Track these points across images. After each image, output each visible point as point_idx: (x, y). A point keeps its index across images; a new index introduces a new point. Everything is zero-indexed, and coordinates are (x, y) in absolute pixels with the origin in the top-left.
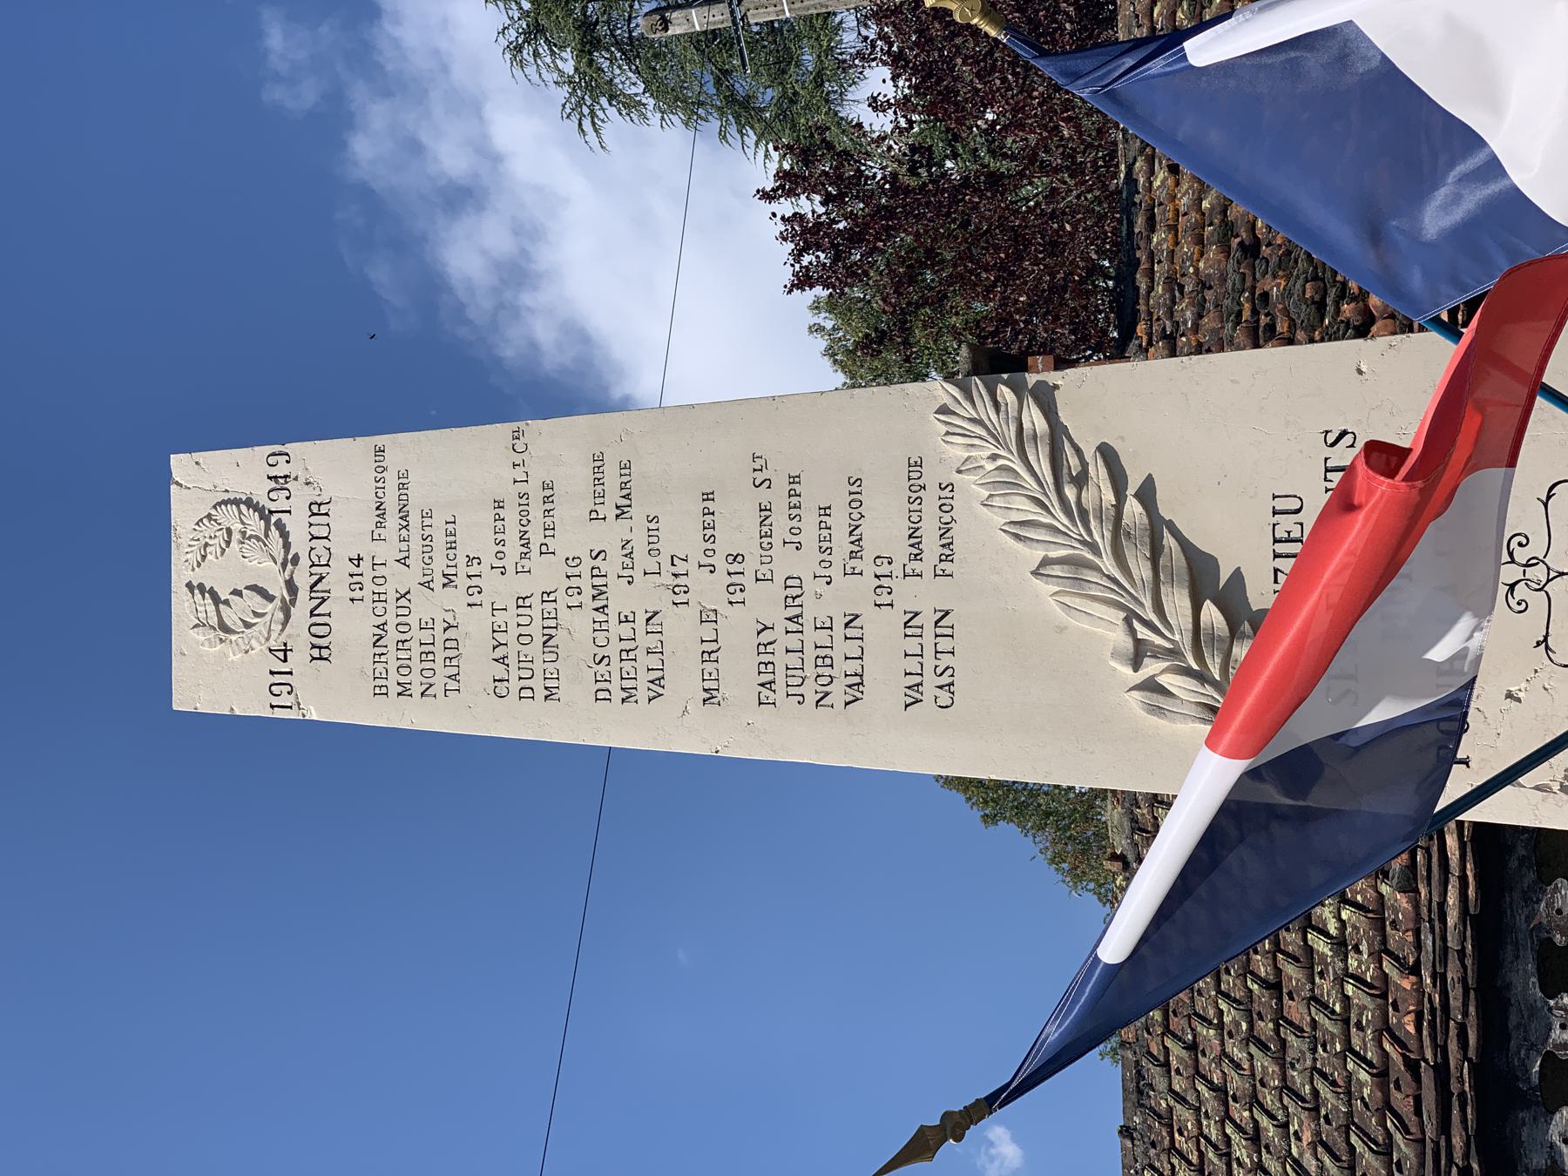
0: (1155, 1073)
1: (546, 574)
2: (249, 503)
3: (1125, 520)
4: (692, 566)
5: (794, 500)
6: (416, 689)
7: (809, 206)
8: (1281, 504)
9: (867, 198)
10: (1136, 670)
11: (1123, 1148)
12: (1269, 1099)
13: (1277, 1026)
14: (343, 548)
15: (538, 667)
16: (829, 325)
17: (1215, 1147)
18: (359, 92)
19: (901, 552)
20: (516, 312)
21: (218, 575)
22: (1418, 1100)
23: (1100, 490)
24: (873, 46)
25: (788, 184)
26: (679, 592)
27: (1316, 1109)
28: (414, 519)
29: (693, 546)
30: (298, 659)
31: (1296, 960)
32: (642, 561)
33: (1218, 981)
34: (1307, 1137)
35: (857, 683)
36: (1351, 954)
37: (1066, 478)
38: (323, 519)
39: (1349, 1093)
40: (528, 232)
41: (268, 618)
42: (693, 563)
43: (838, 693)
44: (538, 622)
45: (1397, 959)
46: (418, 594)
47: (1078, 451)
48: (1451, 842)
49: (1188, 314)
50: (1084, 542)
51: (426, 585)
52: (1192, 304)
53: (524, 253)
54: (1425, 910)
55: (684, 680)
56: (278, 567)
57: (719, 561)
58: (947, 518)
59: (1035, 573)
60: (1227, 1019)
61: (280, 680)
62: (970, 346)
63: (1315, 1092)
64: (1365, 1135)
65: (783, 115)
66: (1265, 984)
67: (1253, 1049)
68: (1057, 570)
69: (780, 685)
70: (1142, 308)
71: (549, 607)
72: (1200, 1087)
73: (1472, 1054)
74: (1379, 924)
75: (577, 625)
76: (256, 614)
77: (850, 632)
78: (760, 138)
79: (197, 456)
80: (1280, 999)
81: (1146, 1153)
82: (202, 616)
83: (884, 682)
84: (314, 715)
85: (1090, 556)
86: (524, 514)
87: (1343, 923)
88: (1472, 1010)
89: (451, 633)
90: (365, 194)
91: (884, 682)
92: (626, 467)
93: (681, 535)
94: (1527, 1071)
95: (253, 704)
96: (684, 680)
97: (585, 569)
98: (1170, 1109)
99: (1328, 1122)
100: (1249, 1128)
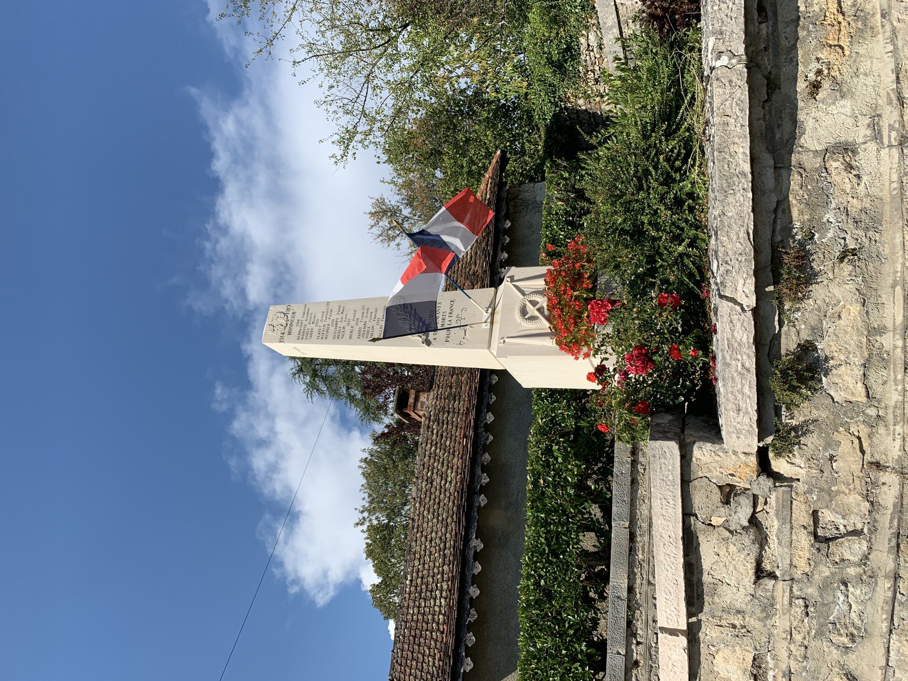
1: (329, 322)
16: (364, 466)
18: (239, 409)
20: (270, 479)
32: (344, 319)
40: (280, 456)
53: (277, 462)
75: (332, 329)
90: (234, 438)
93: (350, 316)
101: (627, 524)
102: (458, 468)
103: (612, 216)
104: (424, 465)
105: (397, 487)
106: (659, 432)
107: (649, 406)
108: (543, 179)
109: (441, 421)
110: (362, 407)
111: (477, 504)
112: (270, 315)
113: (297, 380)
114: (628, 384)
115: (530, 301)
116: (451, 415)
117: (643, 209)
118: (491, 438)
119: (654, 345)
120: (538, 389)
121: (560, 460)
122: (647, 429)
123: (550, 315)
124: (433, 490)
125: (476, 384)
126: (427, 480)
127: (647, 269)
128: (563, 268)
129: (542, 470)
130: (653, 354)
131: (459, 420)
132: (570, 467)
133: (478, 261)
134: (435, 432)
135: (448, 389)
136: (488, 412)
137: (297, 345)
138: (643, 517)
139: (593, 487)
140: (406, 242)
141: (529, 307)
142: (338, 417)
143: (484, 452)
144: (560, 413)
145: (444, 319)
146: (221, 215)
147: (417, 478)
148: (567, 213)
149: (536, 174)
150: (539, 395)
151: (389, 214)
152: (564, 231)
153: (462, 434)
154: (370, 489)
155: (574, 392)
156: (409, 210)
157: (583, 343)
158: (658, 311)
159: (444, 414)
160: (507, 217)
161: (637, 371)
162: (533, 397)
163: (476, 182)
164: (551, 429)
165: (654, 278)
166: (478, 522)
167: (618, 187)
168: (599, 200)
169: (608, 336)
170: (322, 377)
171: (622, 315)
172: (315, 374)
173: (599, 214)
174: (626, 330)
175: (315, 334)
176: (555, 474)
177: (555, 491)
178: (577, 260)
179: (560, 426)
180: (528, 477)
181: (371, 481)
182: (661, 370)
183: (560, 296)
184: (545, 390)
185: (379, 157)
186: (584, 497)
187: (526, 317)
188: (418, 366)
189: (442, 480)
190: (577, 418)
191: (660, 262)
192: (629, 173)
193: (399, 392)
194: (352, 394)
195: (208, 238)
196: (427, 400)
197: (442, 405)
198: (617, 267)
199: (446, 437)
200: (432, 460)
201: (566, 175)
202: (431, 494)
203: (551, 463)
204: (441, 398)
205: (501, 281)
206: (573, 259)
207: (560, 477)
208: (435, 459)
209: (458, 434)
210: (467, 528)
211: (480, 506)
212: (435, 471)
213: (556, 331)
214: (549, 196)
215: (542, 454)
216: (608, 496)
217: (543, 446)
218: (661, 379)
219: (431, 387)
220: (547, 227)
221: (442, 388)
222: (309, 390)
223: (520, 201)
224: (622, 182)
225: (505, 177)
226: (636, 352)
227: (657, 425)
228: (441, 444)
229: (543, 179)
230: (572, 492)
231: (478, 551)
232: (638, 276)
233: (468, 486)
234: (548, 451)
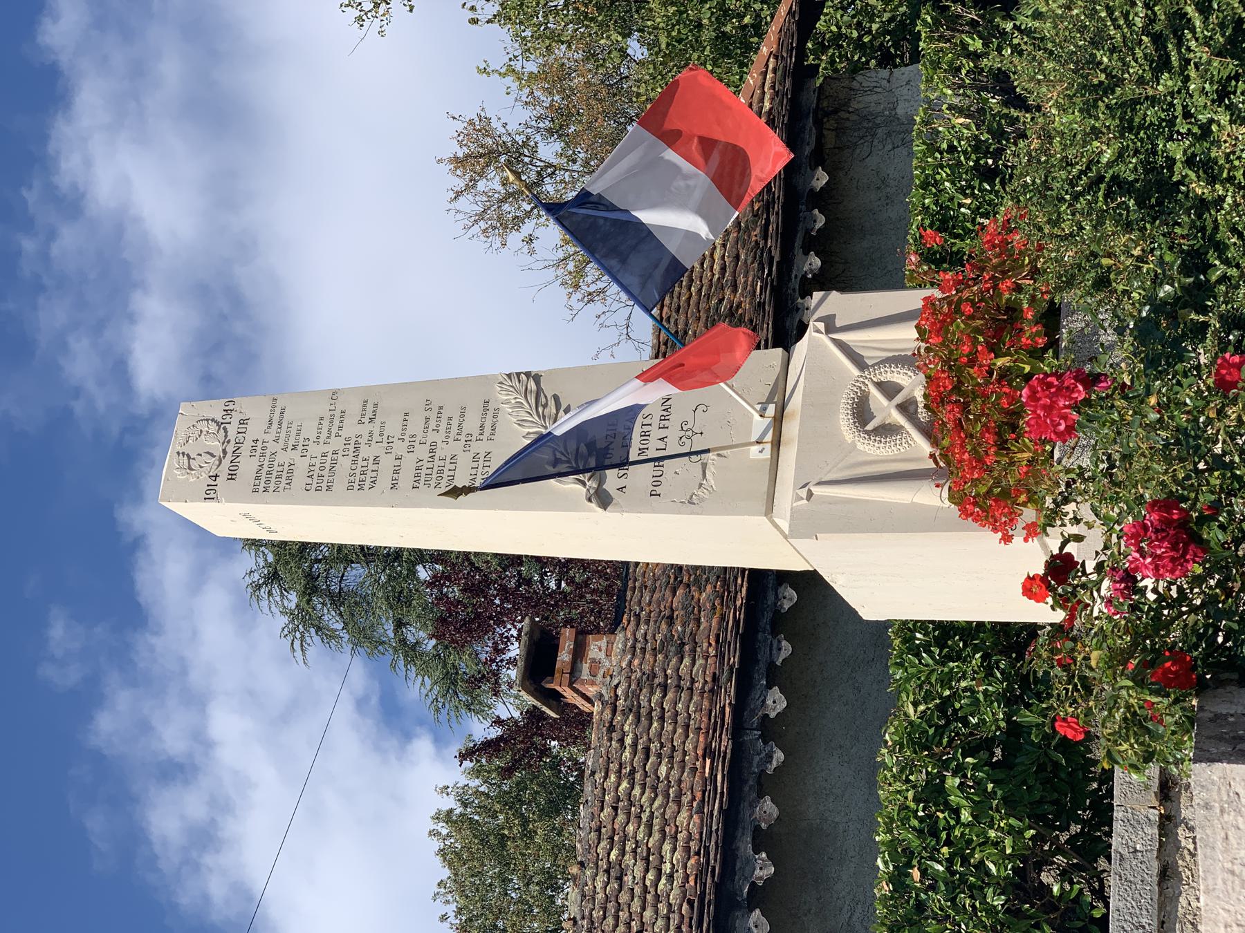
1: (337, 443)
14: (250, 437)
16: (444, 832)
19: (476, 433)
20: (197, 867)
28: (284, 425)
32: (376, 438)
40: (221, 805)
42: (396, 438)
53: (213, 822)
57: (407, 438)
75: (345, 463)
86: (331, 422)
89: (291, 467)
92: (376, 405)
93: (393, 428)
97: (352, 442)
102: (690, 837)
103: (1085, 143)
104: (599, 830)
105: (534, 888)
106: (1220, 738)
107: (1195, 667)
108: (916, 57)
109: (643, 712)
110: (438, 674)
112: (181, 426)
113: (264, 603)
114: (1134, 608)
115: (880, 385)
116: (670, 695)
117: (1171, 123)
118: (779, 756)
119: (1206, 498)
120: (905, 622)
121: (965, 816)
122: (1188, 731)
123: (932, 423)
124: (624, 898)
125: (737, 610)
126: (607, 871)
127: (1183, 288)
128: (966, 294)
129: (916, 843)
130: (1202, 520)
131: (692, 708)
132: (992, 834)
133: (741, 279)
134: (628, 741)
135: (664, 626)
136: (769, 686)
137: (256, 509)
139: (1056, 889)
140: (550, 234)
141: (877, 399)
142: (374, 700)
143: (761, 796)
144: (965, 690)
145: (645, 435)
146: (64, 166)
147: (582, 864)
148: (978, 146)
149: (896, 45)
150: (909, 640)
151: (503, 159)
152: (973, 195)
153: (701, 745)
154: (462, 893)
155: (1003, 629)
156: (558, 146)
157: (1023, 498)
158: (1217, 402)
159: (652, 693)
160: (819, 158)
161: (1157, 568)
162: (890, 646)
163: (735, 68)
164: (940, 731)
165: (1204, 310)
167: (1100, 63)
168: (1050, 97)
169: (1081, 475)
170: (331, 595)
171: (1115, 416)
172: (311, 588)
173: (1050, 138)
174: (1127, 458)
175: (300, 478)
176: (952, 855)
177: (953, 900)
178: (1004, 273)
179: (966, 723)
180: (879, 862)
181: (463, 870)
182: (1227, 567)
183: (960, 370)
184: (922, 625)
185: (473, 8)
186: (1031, 917)
187: (870, 427)
188: (584, 564)
189: (647, 871)
190: (1011, 701)
191: (1220, 269)
192: (1130, 25)
193: (531, 634)
194: (411, 639)
195: (27, 225)
196: (608, 655)
197: (647, 668)
198: (1102, 282)
199: (659, 756)
200: (621, 818)
201: (976, 45)
202: (619, 907)
203: (942, 824)
204: (644, 650)
205: (802, 329)
206: (995, 268)
207: (965, 861)
208: (629, 814)
209: (689, 746)
212: (630, 846)
213: (948, 464)
214: (929, 101)
215: (917, 800)
216: (1097, 914)
217: (919, 778)
218: (1228, 592)
220: (925, 185)
221: (647, 622)
222: (296, 628)
223: (854, 117)
224: (1113, 50)
225: (813, 52)
226: (1154, 517)
227: (1217, 718)
228: (646, 774)
229: (916, 57)
230: (998, 902)
232: (1159, 307)
233: (718, 887)
234: (933, 793)
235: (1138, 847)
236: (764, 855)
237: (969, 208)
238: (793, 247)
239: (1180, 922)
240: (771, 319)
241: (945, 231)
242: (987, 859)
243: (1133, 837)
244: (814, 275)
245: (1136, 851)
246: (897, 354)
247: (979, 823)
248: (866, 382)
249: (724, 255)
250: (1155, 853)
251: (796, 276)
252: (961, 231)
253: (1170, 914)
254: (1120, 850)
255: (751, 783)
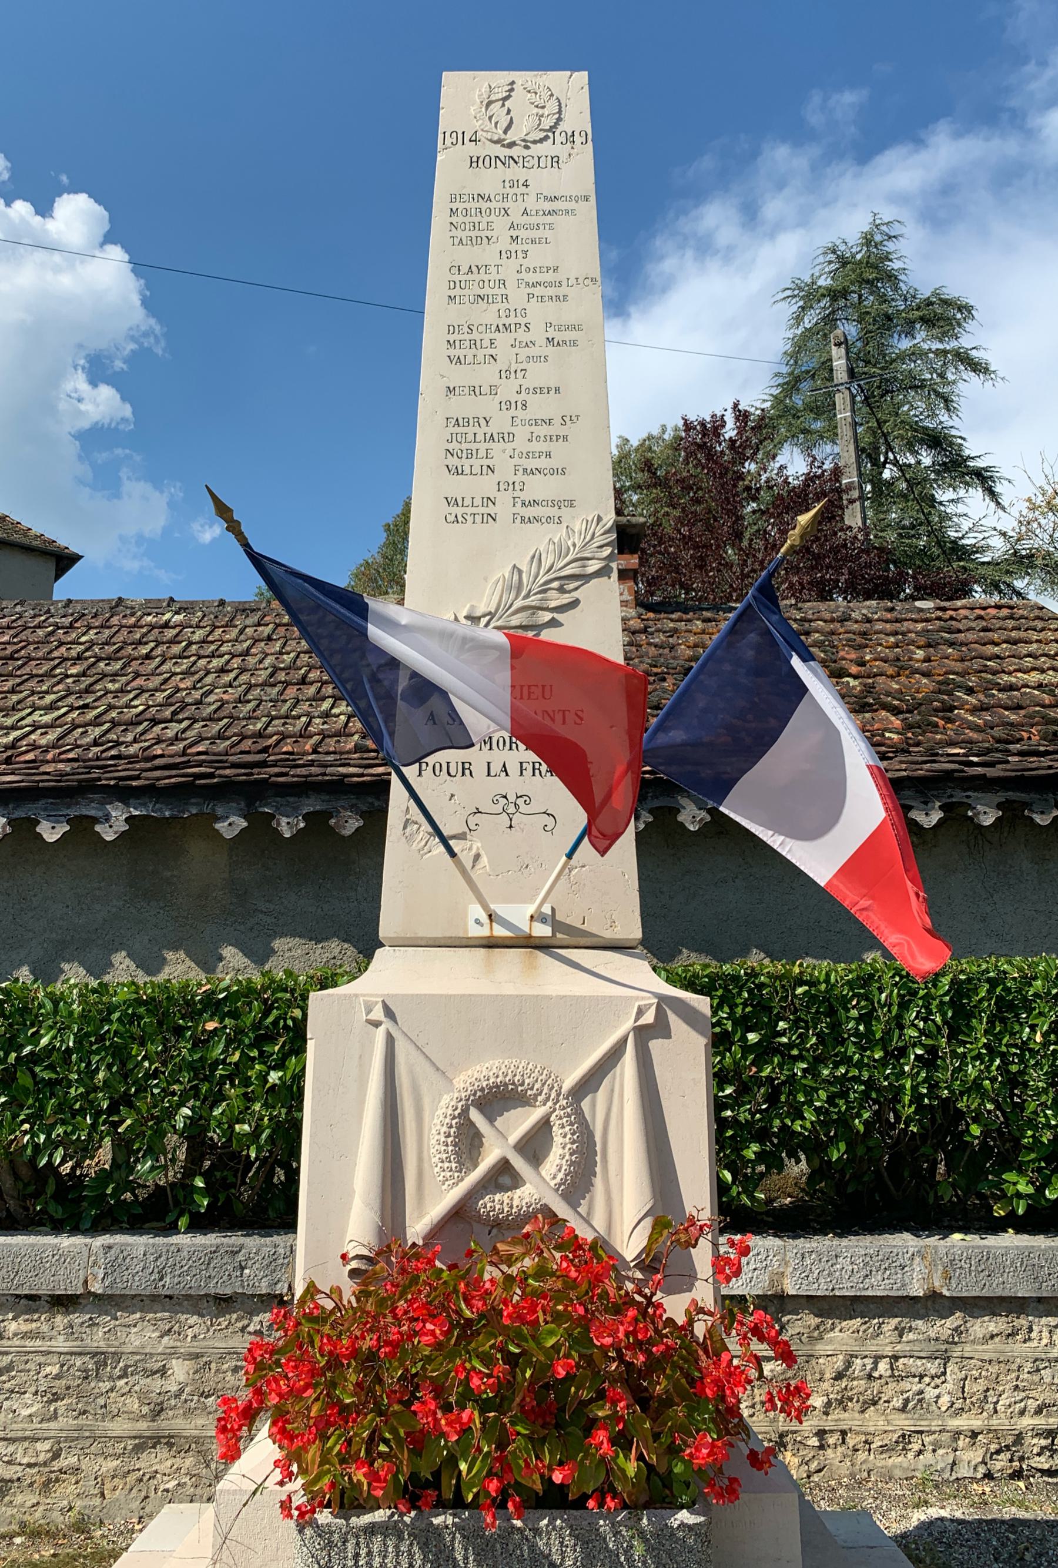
0: (254, 618)
1: (517, 296)
2: (559, 119)
3: (540, 612)
4: (521, 381)
5: (554, 438)
6: (454, 220)
7: (730, 431)
8: (547, 689)
9: (733, 462)
10: (465, 617)
11: (213, 601)
12: (244, 677)
13: (283, 683)
15: (466, 292)
16: (666, 437)
17: (217, 650)
18: (815, 151)
19: (526, 496)
20: (682, 247)
21: (519, 101)
22: (248, 752)
23: (556, 600)
24: (819, 467)
25: (742, 416)
26: (507, 373)
27: (240, 702)
28: (549, 219)
29: (530, 382)
30: (471, 149)
31: (318, 693)
32: (524, 353)
33: (305, 652)
34: (226, 697)
35: (458, 472)
36: (322, 720)
37: (563, 582)
38: (549, 165)
39: (250, 718)
40: (728, 255)
41: (494, 130)
43: (453, 461)
44: (491, 292)
45: (321, 742)
46: (509, 220)
47: (576, 589)
48: (381, 770)
49: (657, 640)
50: (530, 591)
51: (512, 226)
52: (663, 642)
54: (346, 756)
55: (459, 376)
56: (523, 136)
57: (520, 398)
58: (544, 520)
59: (514, 566)
60: (285, 657)
61: (460, 138)
62: (646, 523)
63: (249, 701)
64: (228, 726)
65: (787, 410)
66: (305, 677)
67: (270, 670)
68: (516, 577)
69: (457, 430)
70: (662, 615)
71: (499, 299)
72: (248, 642)
73: (273, 779)
74: (338, 734)
75: (489, 315)
76: (496, 123)
77: (485, 468)
78: (775, 397)
79: (587, 87)
80: (297, 684)
81: (212, 613)
82: (496, 90)
83: (458, 486)
84: (440, 158)
85: (523, 594)
86: (551, 284)
87: (338, 716)
88: (295, 779)
89: (485, 240)
90: (755, 154)
91: (458, 486)
92: (574, 343)
93: (538, 375)
94: (265, 806)
95: (447, 121)
96: (459, 376)
98: (236, 626)
99: (234, 708)
100: (228, 667)
101: (96, 1288)
111: (219, 811)
115: (544, 1126)
138: (121, 1333)
143: (363, 815)
166: (172, 817)
187: (475, 1115)
210: (151, 792)
211: (218, 819)
219: (649, 608)
222: (801, 289)
231: (98, 828)
235: (247, 1271)
236: (302, 825)
237: (1029, 1039)
238: (1007, 790)
239: (172, 1317)
240: (911, 774)
241: (999, 1009)
242: (228, 1105)
243: (257, 1265)
244: (971, 819)
245: (242, 1268)
246: (598, 1148)
247: (267, 1093)
248: (550, 1104)
249: (1028, 686)
250: (240, 1291)
251: (968, 797)
252: (998, 1029)
253: (180, 1304)
254: (243, 1251)
255: (376, 804)
